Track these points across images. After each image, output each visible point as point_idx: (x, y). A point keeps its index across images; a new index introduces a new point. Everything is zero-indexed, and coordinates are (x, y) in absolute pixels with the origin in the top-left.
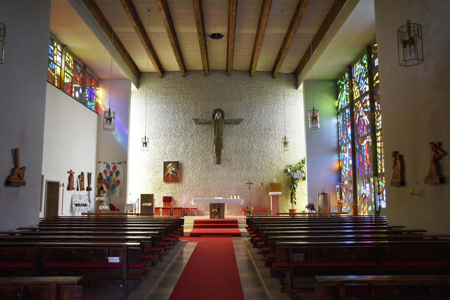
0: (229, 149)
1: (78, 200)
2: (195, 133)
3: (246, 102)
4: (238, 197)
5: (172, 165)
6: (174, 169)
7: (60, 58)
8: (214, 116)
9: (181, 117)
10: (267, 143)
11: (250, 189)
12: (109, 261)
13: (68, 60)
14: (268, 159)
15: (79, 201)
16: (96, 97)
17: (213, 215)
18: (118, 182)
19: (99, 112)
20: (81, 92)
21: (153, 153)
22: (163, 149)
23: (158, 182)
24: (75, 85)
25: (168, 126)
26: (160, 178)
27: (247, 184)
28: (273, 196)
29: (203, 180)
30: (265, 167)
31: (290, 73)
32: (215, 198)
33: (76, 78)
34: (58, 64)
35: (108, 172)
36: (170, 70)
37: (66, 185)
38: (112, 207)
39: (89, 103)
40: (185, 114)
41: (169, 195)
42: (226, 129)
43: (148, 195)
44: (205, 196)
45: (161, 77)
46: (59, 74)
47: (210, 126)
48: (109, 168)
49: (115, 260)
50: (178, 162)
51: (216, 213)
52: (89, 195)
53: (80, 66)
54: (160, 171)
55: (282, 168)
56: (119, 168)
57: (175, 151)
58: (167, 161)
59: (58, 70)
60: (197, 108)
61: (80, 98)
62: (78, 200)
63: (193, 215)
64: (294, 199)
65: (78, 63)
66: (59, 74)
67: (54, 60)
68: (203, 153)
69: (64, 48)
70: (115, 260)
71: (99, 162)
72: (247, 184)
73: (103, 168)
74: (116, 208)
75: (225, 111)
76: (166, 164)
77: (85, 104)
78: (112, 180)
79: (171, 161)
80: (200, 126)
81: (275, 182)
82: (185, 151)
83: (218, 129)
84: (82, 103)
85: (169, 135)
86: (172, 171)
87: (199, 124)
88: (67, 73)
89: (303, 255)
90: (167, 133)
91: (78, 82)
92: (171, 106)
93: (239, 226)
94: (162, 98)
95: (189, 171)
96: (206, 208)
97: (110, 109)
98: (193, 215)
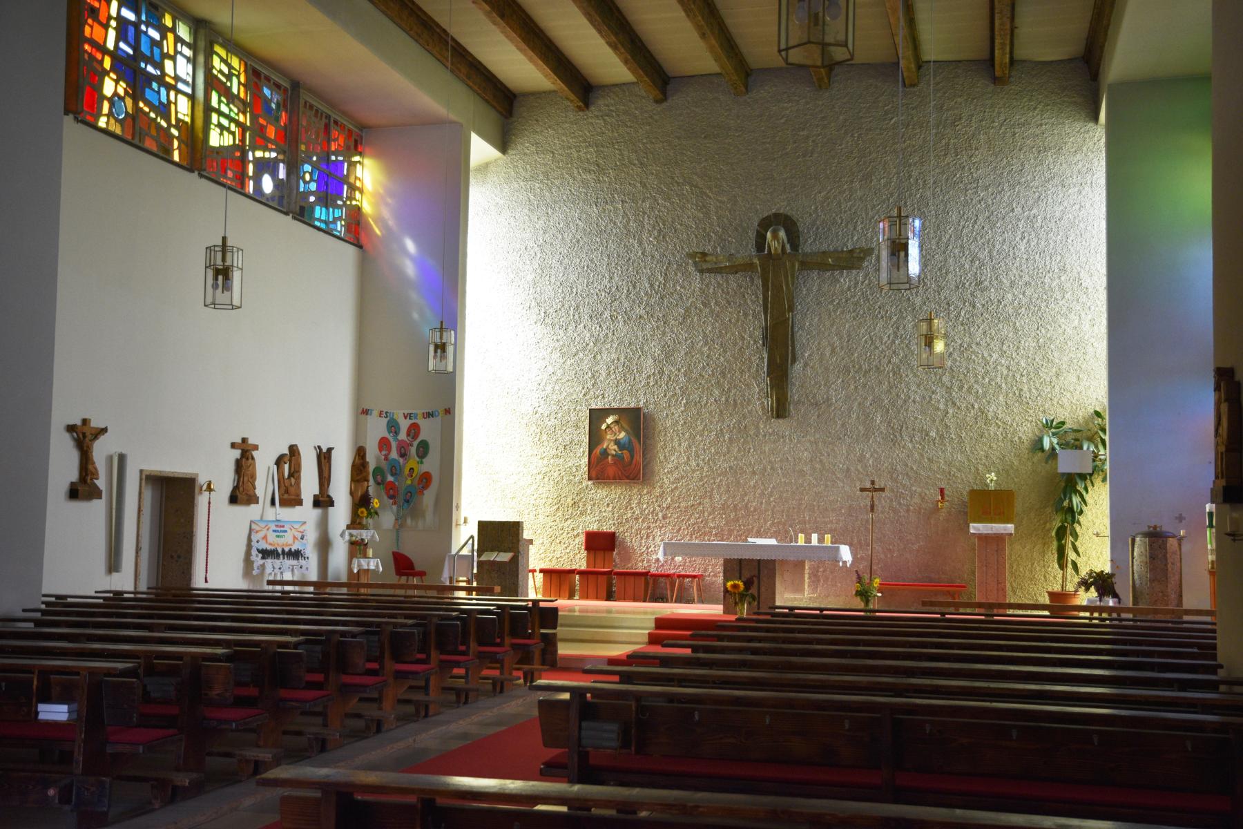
1: (272, 537)
2: (699, 305)
3: (888, 184)
4: (828, 537)
5: (616, 422)
6: (623, 435)
7: (190, 67)
9: (648, 249)
10: (967, 339)
12: (41, 716)
13: (225, 70)
14: (971, 399)
15: (274, 542)
16: (353, 188)
18: (426, 479)
19: (363, 240)
20: (282, 174)
21: (554, 378)
23: (570, 482)
24: (259, 154)
25: (606, 281)
26: (578, 468)
27: (862, 490)
29: (724, 474)
30: (959, 427)
31: (1070, 60)
33: (262, 129)
34: (181, 86)
35: (394, 445)
36: (677, 74)
37: (225, 482)
38: (402, 564)
39: (319, 212)
40: (662, 236)
41: (606, 528)
42: (812, 289)
44: (730, 531)
45: (580, 108)
46: (188, 119)
47: (752, 279)
48: (397, 433)
49: (55, 712)
50: (639, 409)
52: (323, 525)
53: (278, 86)
54: (579, 444)
55: (1026, 432)
56: (429, 430)
57: (628, 372)
58: (600, 406)
59: (183, 108)
60: (707, 215)
61: (281, 198)
62: (272, 537)
64: (1072, 555)
65: (268, 79)
66: (188, 119)
67: (164, 74)
68: (724, 376)
69: (202, 32)
70: (55, 712)
71: (366, 412)
72: (862, 490)
73: (376, 429)
74: (418, 568)
75: (803, 225)
76: (596, 416)
77: (302, 214)
78: (407, 471)
79: (615, 405)
81: (992, 486)
82: (661, 372)
84: (286, 214)
85: (607, 314)
86: (617, 442)
87: (710, 271)
88: (220, 113)
89: (614, 727)
91: (270, 141)
92: (616, 209)
94: (585, 183)
95: (676, 444)
97: (224, 239)
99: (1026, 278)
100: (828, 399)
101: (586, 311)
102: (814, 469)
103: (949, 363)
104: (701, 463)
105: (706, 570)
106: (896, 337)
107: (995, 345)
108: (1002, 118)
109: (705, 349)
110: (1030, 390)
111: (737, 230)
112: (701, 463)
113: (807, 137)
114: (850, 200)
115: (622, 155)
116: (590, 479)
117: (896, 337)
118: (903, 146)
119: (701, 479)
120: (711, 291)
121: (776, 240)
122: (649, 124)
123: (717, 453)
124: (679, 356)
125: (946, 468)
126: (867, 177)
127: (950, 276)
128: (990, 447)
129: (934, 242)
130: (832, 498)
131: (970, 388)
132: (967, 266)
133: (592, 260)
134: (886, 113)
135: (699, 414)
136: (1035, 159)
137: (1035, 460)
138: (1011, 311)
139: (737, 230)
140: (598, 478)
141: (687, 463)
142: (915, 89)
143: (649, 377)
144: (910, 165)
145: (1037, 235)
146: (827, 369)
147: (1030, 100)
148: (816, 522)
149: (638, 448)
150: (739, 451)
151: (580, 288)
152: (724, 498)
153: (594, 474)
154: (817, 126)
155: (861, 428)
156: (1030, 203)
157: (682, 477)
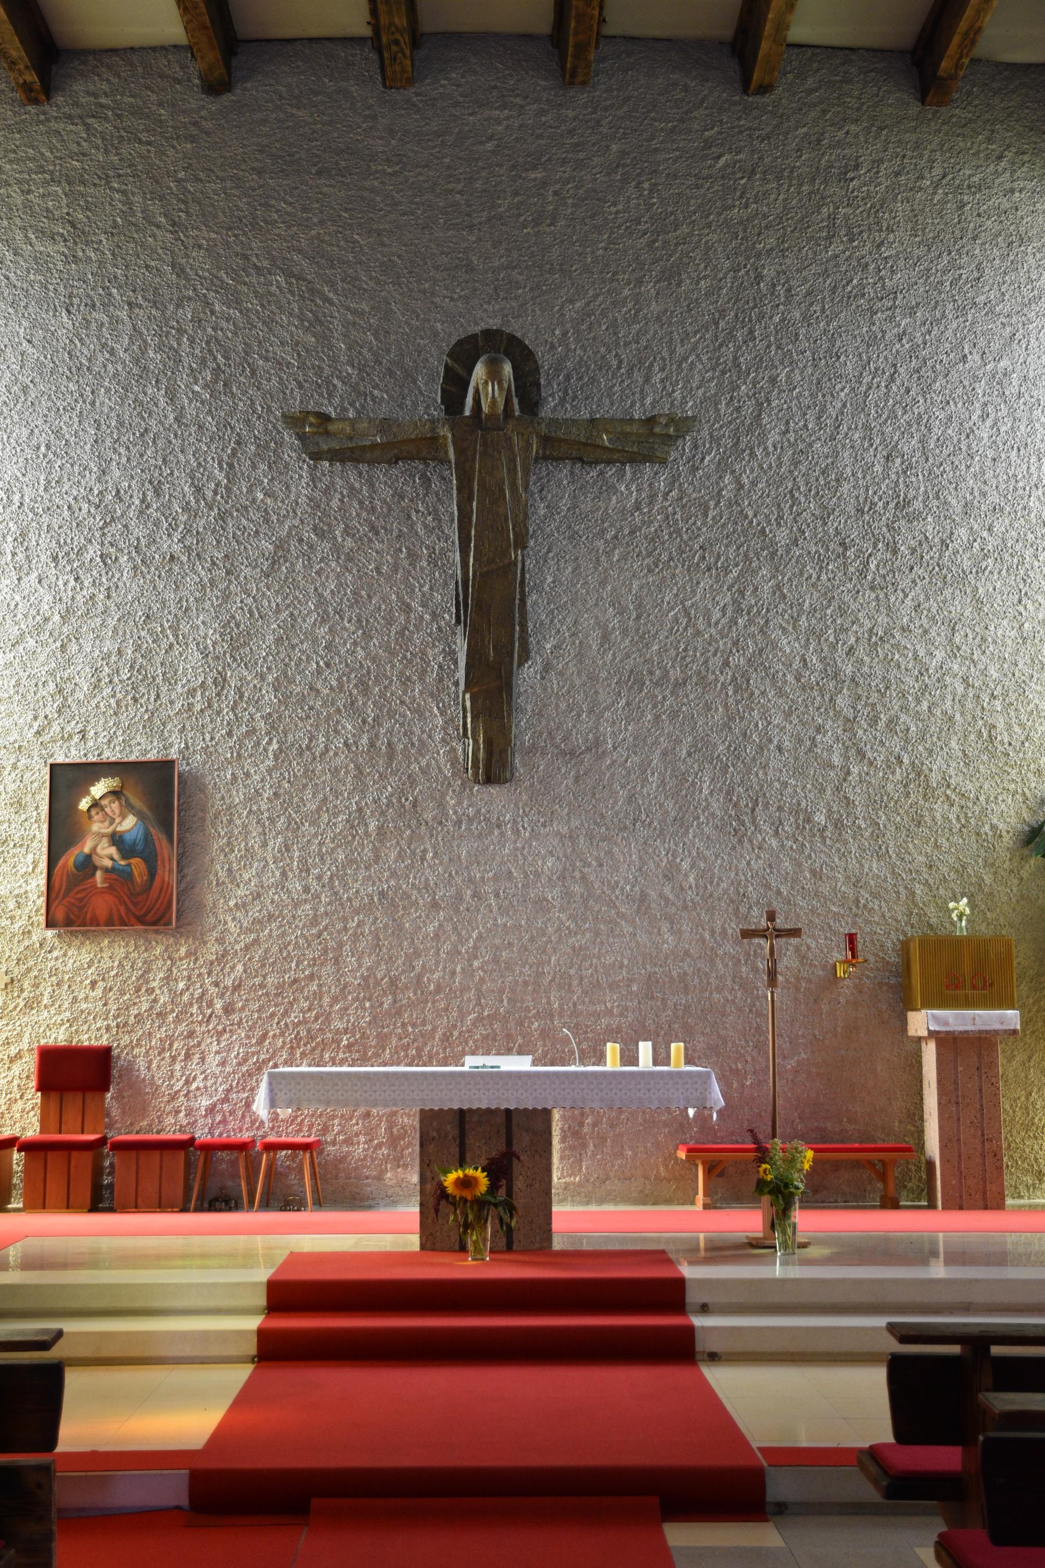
0: (580, 657)
2: (309, 535)
4: (677, 1048)
5: (115, 794)
8: (455, 384)
9: (190, 411)
10: (882, 619)
11: (772, 981)
14: (895, 744)
17: (452, 1218)
25: (91, 479)
28: (949, 1043)
29: (368, 908)
30: (871, 802)
32: (471, 1062)
40: (221, 383)
41: (87, 1039)
42: (558, 502)
47: (426, 481)
50: (167, 765)
51: (481, 1204)
54: (24, 844)
57: (140, 681)
58: (74, 755)
60: (324, 338)
63: (286, 1205)
68: (366, 691)
75: (545, 360)
76: (66, 781)
79: (110, 755)
80: (344, 478)
82: (221, 682)
83: (493, 495)
85: (93, 551)
86: (116, 839)
87: (337, 456)
90: (79, 540)
92: (115, 321)
93: (702, 1344)
94: (40, 262)
95: (255, 842)
96: (393, 1141)
98: (280, 1198)
99: (994, 498)
100: (597, 743)
101: (43, 545)
102: (568, 894)
103: (849, 670)
104: (315, 886)
105: (325, 1130)
106: (739, 610)
107: (938, 633)
108: (937, 171)
109: (322, 631)
110: (1009, 727)
111: (391, 373)
112: (315, 886)
113: (544, 184)
114: (635, 319)
115: (129, 203)
116: (49, 924)
117: (739, 610)
118: (744, 214)
119: (314, 921)
120: (335, 503)
121: (486, 386)
122: (192, 139)
123: (351, 862)
124: (263, 646)
125: (850, 892)
126: (671, 276)
127: (846, 487)
128: (937, 846)
129: (811, 416)
130: (609, 959)
131: (892, 722)
132: (878, 468)
133: (58, 433)
134: (708, 144)
135: (309, 773)
136: (1003, 257)
137: (1024, 874)
138: (967, 564)
139: (391, 373)
140: (68, 923)
141: (281, 885)
142: (767, 99)
143: (192, 692)
144: (758, 256)
145: (1012, 412)
146: (593, 678)
147: (989, 140)
148: (575, 1013)
149: (167, 852)
150: (400, 857)
151: (29, 493)
152: (367, 962)
153: (60, 915)
154: (564, 162)
155: (669, 804)
156: (995, 346)
157: (271, 917)
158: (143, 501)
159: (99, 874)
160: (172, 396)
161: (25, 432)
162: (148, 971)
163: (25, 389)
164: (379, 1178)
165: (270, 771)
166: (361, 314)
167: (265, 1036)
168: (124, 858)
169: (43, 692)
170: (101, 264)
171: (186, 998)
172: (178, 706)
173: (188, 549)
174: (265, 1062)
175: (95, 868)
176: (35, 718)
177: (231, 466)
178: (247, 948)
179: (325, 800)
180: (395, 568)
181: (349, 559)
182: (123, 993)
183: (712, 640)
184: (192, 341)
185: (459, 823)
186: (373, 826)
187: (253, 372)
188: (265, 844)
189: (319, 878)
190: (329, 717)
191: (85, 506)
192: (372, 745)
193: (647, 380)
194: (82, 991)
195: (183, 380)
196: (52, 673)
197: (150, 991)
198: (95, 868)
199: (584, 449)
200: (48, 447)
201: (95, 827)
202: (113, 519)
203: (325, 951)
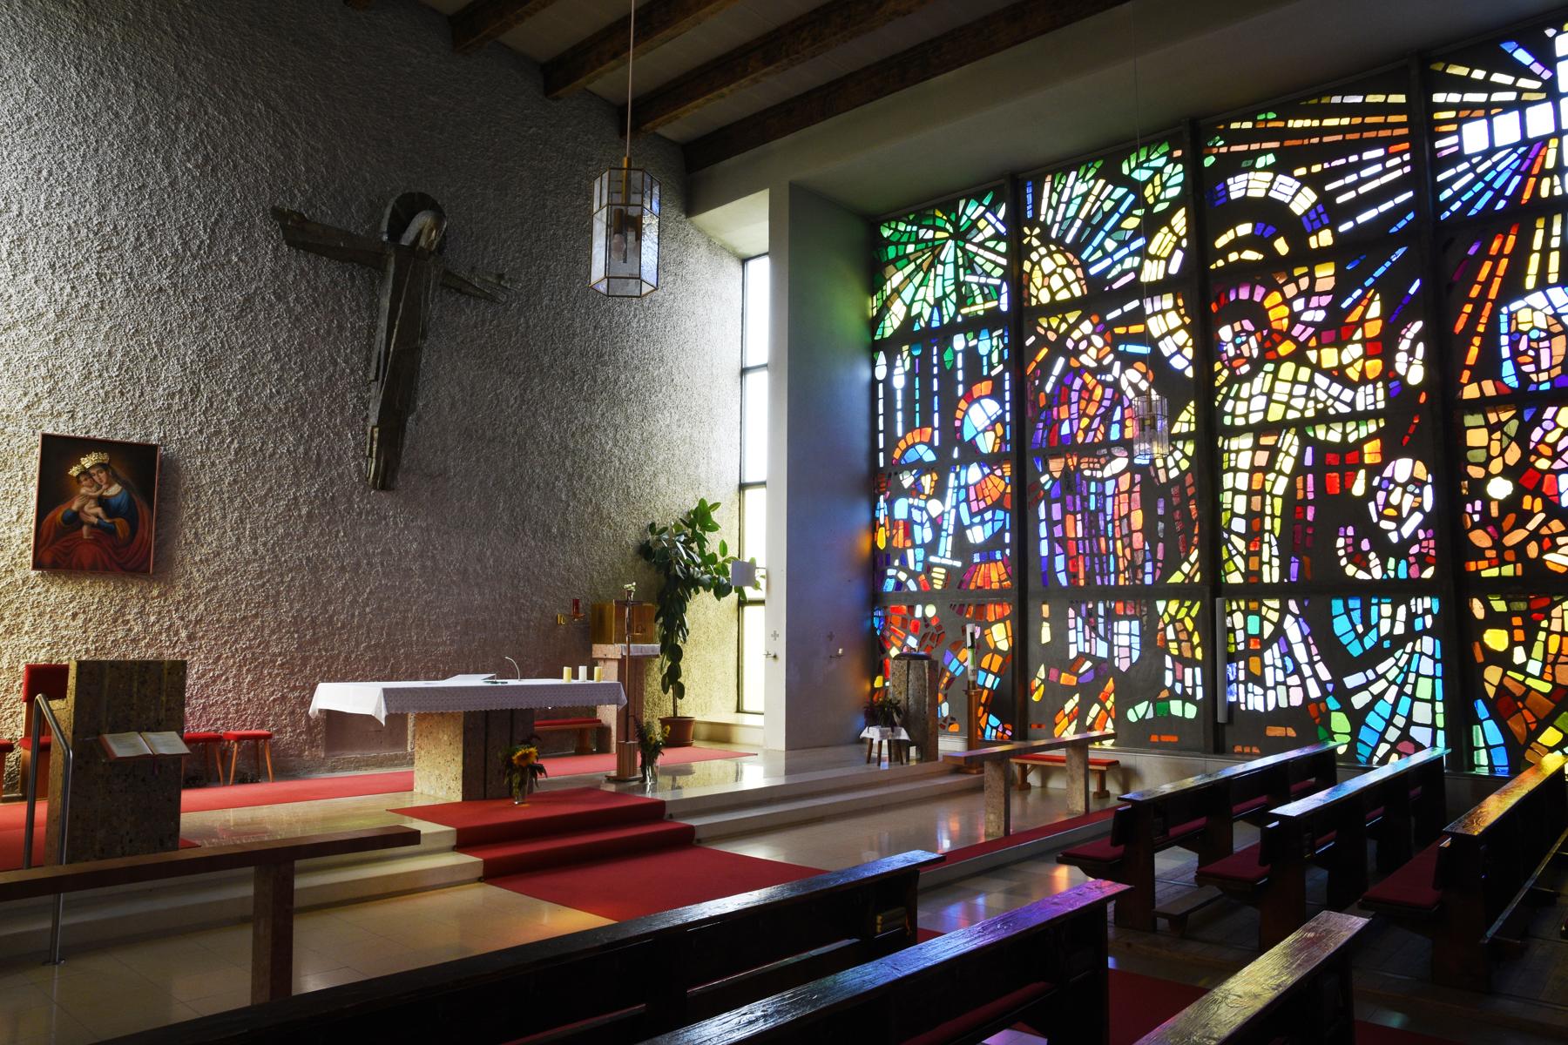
5: (101, 466)
6: (115, 489)
9: (183, 182)
22: (37, 349)
43: (144, 666)
47: (352, 278)
55: (632, 536)
58: (63, 429)
68: (304, 415)
76: (58, 452)
82: (195, 391)
85: (89, 269)
86: (102, 501)
95: (216, 514)
102: (423, 567)
119: (260, 575)
120: (290, 278)
123: (287, 534)
130: (446, 610)
148: (425, 644)
150: (321, 534)
152: (297, 606)
153: (47, 558)
158: (137, 239)
159: (85, 528)
160: (168, 166)
161: (27, 156)
162: (124, 607)
163: (29, 120)
164: (300, 755)
165: (231, 463)
166: (317, 151)
167: (219, 658)
168: (108, 516)
169: (32, 373)
170: (111, 43)
171: (156, 628)
172: (159, 403)
173: (175, 285)
174: (219, 676)
175: (82, 524)
176: (25, 394)
177: (213, 231)
178: (208, 592)
179: (271, 489)
180: (329, 333)
181: (297, 319)
182: (101, 623)
183: (509, 417)
184: (188, 129)
185: (360, 514)
186: (304, 512)
187: (235, 167)
188: (224, 517)
189: (265, 544)
190: (277, 430)
191: (84, 231)
192: (306, 453)
193: (486, 248)
194: (71, 622)
195: (178, 156)
196: (44, 360)
197: (126, 622)
198: (82, 524)
199: (455, 285)
200: (50, 173)
201: (83, 491)
202: (109, 248)
203: (267, 597)
